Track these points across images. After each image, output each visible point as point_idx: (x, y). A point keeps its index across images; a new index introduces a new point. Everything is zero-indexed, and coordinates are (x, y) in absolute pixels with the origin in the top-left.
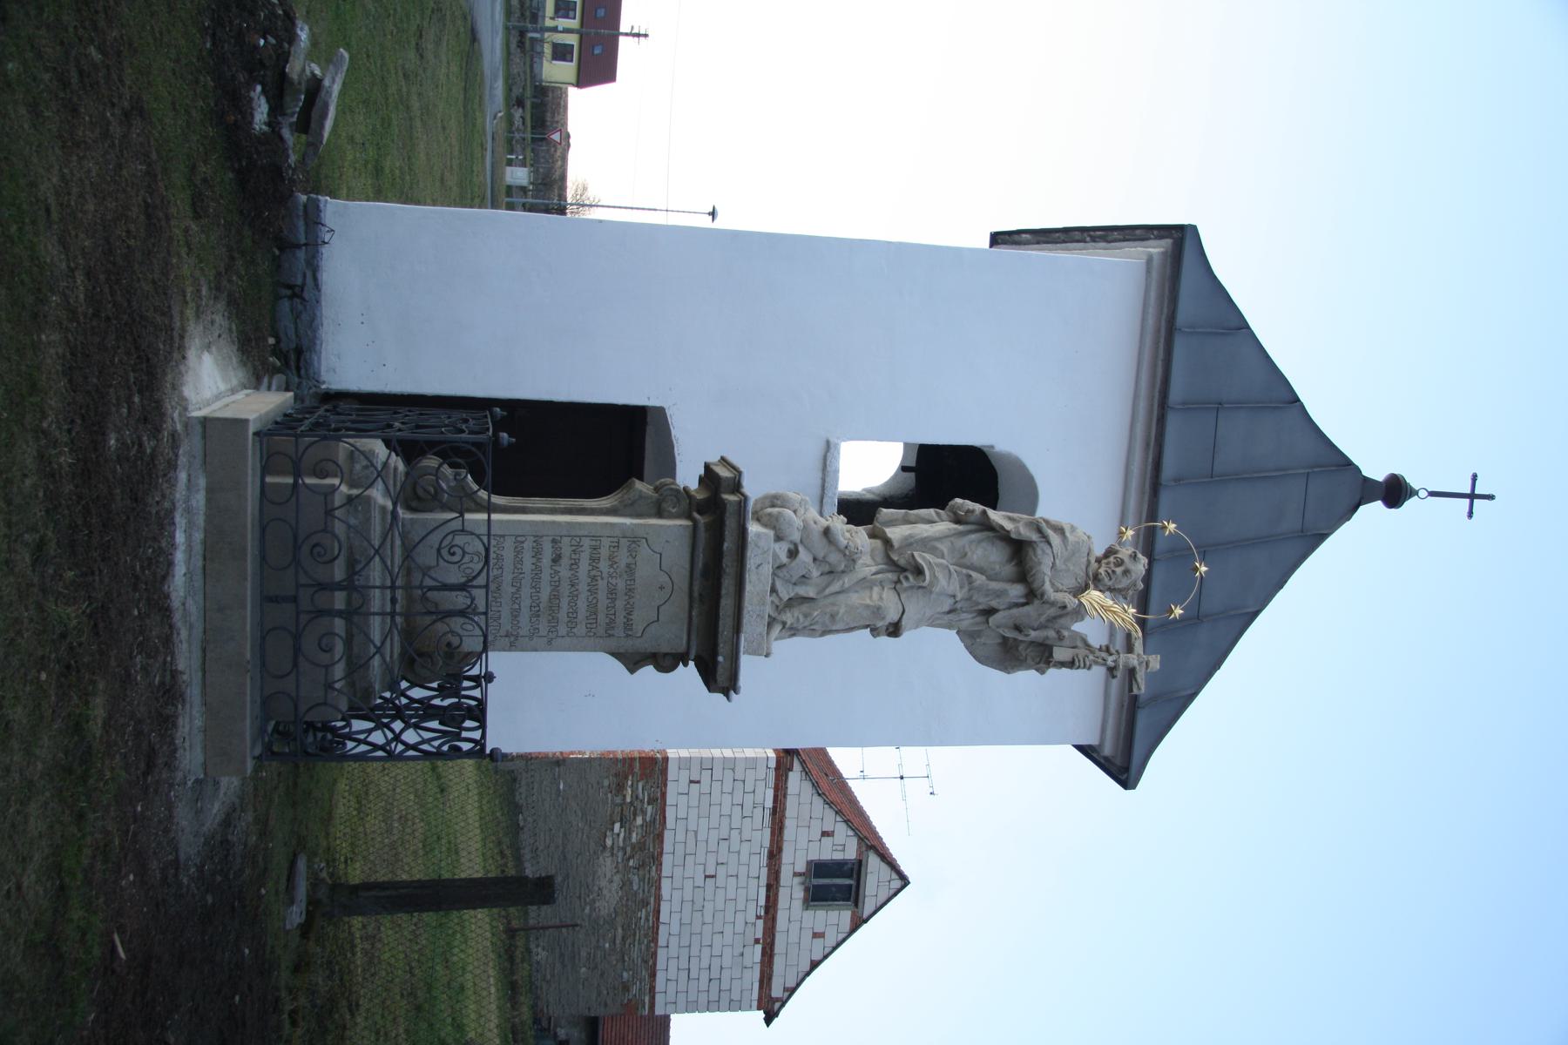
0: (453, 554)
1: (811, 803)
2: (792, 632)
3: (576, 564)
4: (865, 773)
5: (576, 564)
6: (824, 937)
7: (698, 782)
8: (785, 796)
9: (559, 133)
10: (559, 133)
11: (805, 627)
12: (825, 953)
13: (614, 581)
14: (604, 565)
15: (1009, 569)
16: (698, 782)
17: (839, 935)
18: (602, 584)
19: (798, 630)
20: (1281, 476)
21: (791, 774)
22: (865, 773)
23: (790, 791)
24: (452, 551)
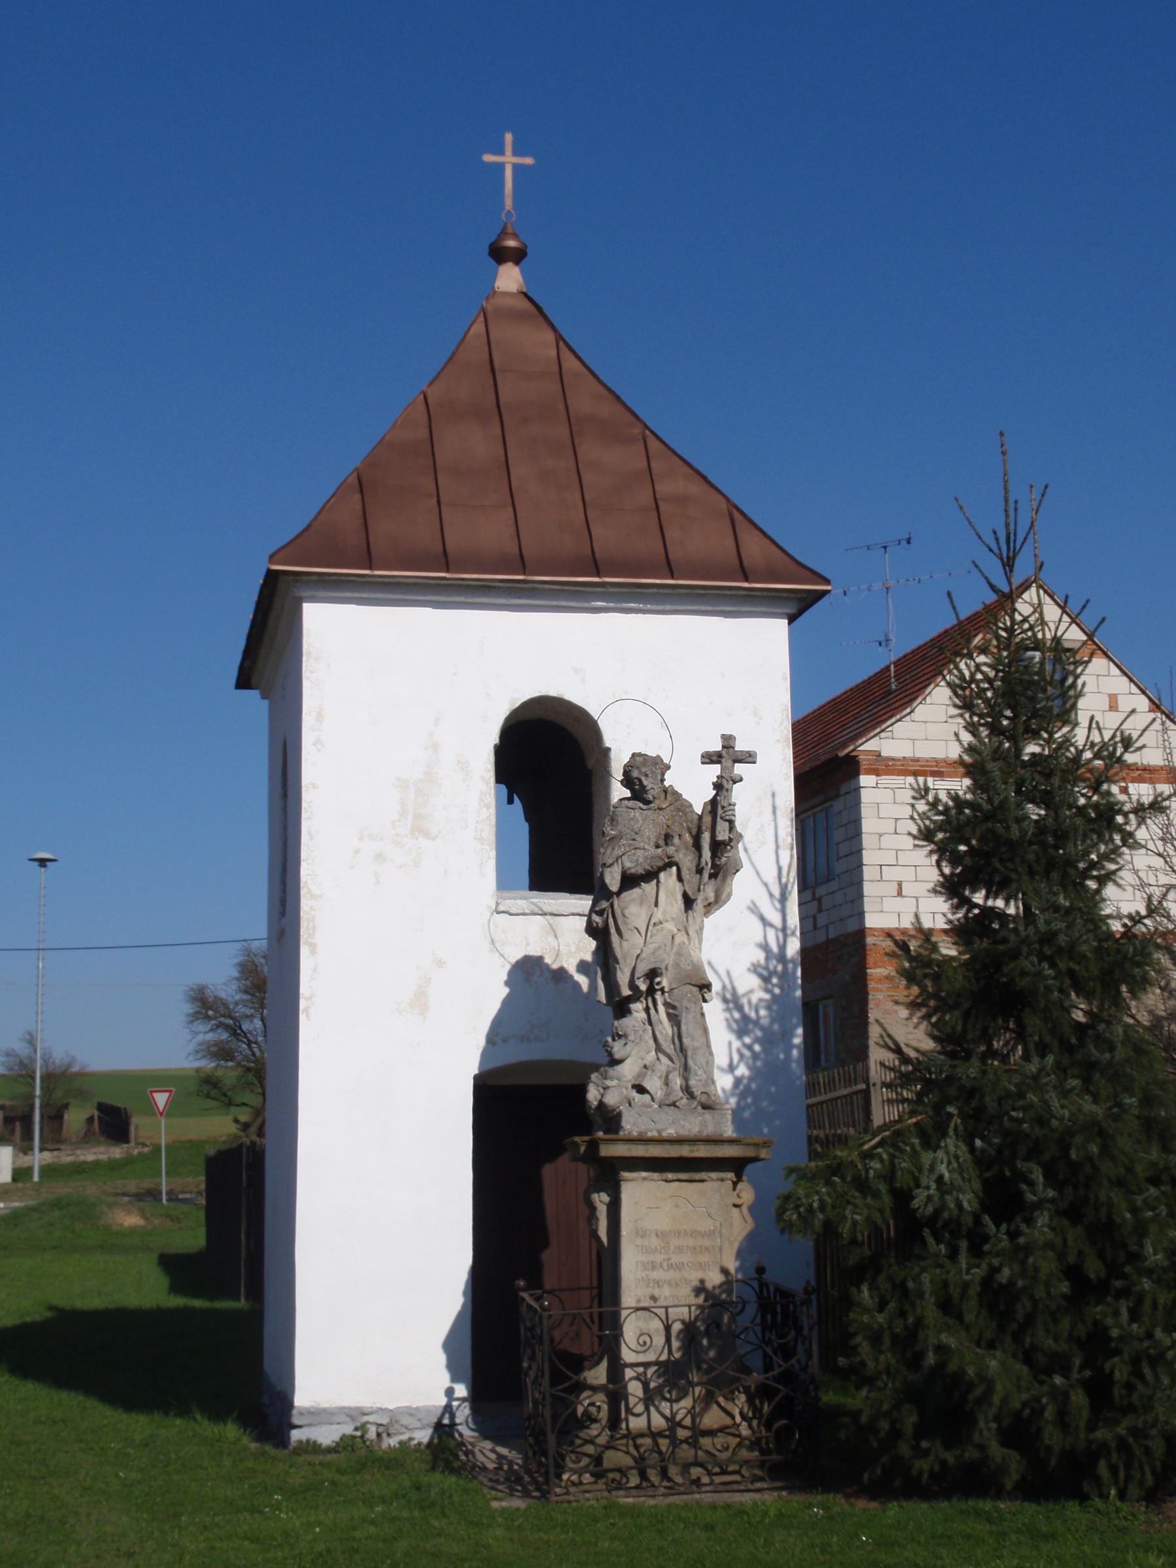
0: (645, 1343)
1: (925, 722)
2: (710, 1081)
3: (658, 1282)
4: (882, 639)
5: (658, 1282)
6: (1116, 695)
7: (900, 885)
8: (916, 760)
9: (155, 1095)
10: (155, 1095)
11: (705, 1072)
12: (1139, 692)
13: (672, 1248)
14: (658, 1258)
15: (649, 888)
16: (900, 885)
17: (1112, 674)
18: (675, 1259)
19: (708, 1078)
20: (559, 590)
21: (885, 753)
22: (882, 639)
23: (908, 754)
24: (641, 1343)
